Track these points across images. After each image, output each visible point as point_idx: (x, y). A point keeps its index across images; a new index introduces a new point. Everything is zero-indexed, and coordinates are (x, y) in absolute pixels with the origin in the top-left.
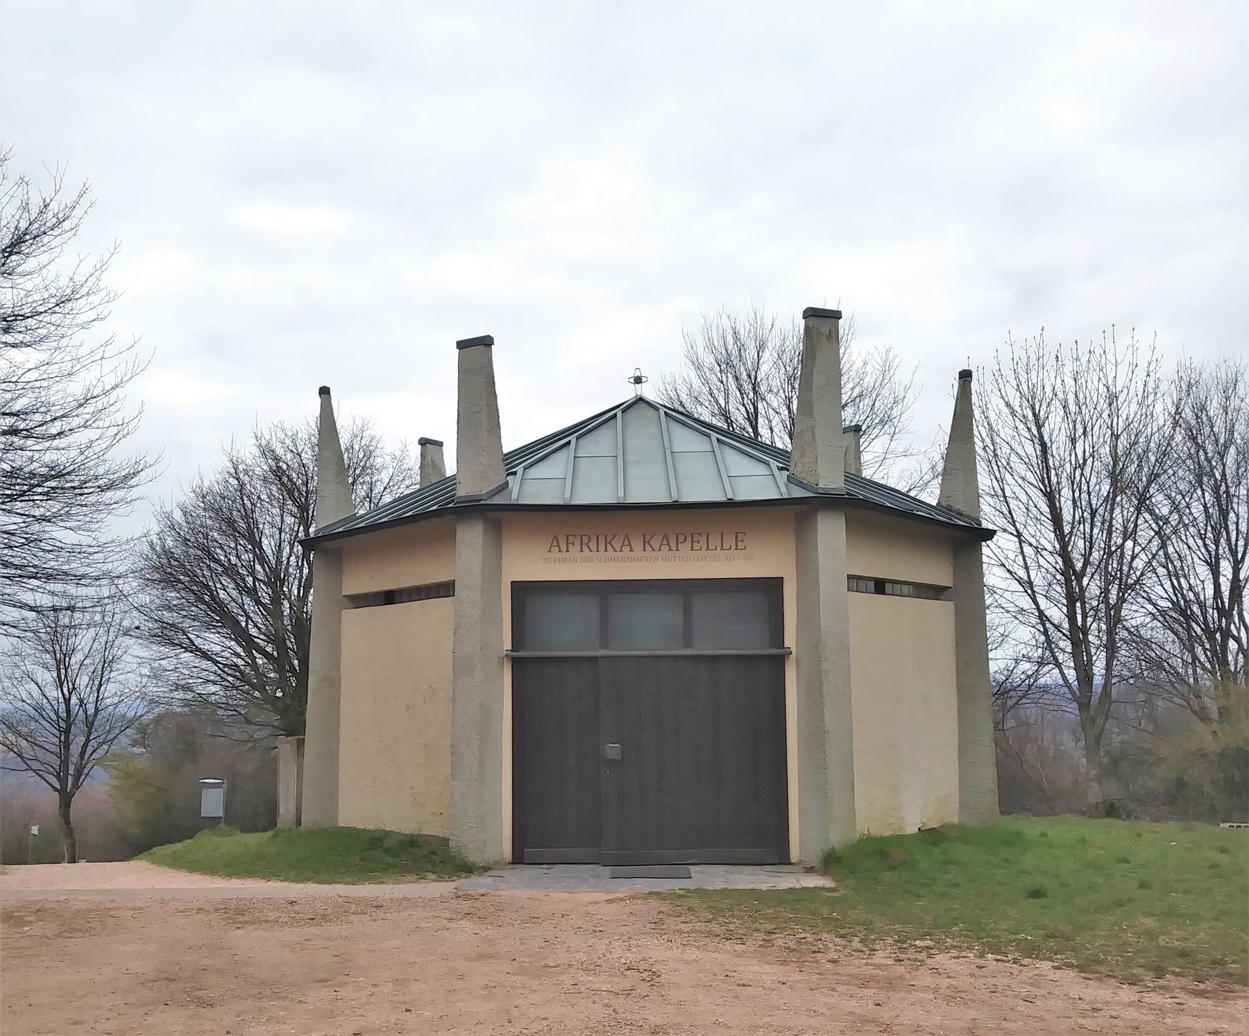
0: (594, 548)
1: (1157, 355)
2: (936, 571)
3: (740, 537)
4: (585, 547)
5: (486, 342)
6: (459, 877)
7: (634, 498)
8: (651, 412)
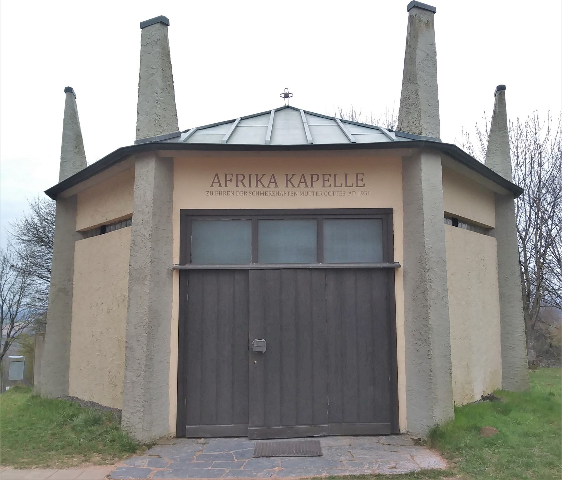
0: (247, 184)
2: (484, 215)
3: (360, 177)
4: (240, 183)
5: (163, 22)
6: (120, 458)
7: (279, 141)
8: (296, 113)
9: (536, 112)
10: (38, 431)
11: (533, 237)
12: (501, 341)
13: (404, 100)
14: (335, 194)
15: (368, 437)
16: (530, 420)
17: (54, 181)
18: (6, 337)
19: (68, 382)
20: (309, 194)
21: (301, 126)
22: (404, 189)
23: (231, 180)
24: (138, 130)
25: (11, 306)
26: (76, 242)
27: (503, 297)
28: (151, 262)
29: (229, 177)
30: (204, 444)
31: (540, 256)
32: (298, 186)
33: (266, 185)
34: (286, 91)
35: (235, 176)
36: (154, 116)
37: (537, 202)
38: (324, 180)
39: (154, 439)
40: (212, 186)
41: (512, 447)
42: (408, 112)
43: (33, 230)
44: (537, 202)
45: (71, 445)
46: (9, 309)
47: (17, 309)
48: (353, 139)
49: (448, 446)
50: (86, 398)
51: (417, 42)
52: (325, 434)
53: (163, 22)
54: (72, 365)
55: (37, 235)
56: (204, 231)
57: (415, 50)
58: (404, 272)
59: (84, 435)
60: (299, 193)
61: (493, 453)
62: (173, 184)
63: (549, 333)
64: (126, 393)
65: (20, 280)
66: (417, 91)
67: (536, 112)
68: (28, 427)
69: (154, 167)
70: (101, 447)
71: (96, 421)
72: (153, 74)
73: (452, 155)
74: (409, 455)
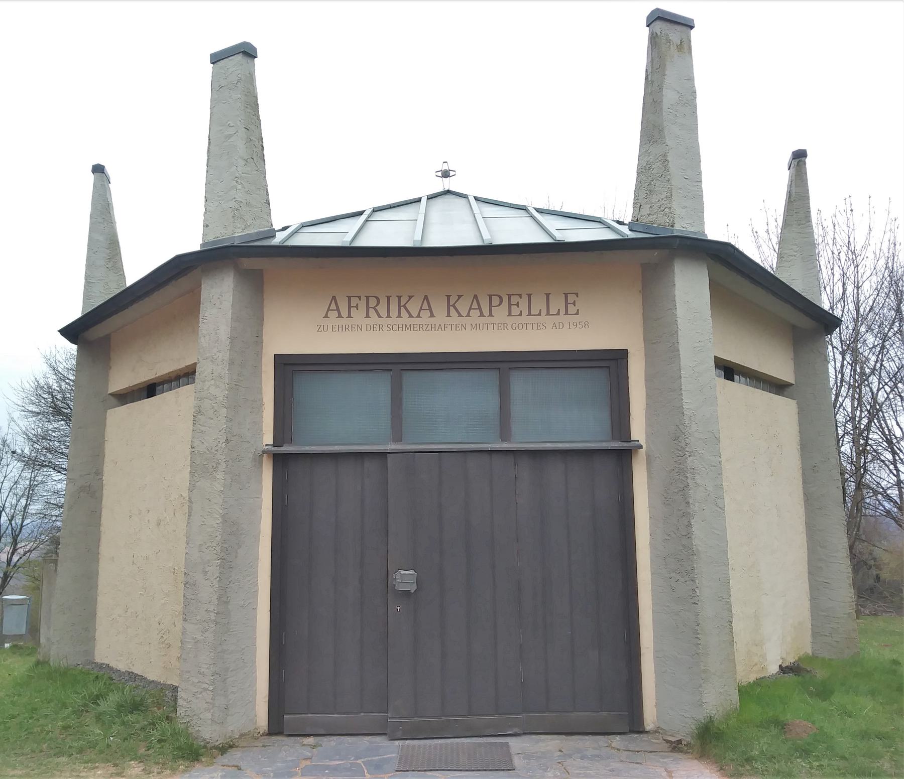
0: (384, 313)
1: (892, 216)
2: (776, 363)
3: (571, 298)
4: (372, 311)
5: (247, 52)
7: (435, 240)
8: (462, 201)
9: (848, 199)
10: (42, 721)
11: (848, 403)
12: (809, 573)
13: (643, 170)
14: (530, 327)
15: (591, 737)
16: (869, 710)
17: (74, 312)
18: (5, 565)
19: (94, 639)
20: (485, 327)
21: (471, 219)
22: (646, 319)
23: (357, 307)
24: (206, 226)
25: (13, 517)
26: (110, 412)
27: (811, 502)
28: (227, 441)
29: (354, 302)
30: (314, 747)
31: (859, 436)
32: (468, 315)
33: (415, 314)
34: (445, 167)
35: (364, 299)
36: (233, 204)
37: (851, 348)
38: (510, 305)
39: (230, 737)
40: (326, 316)
41: (843, 758)
42: (650, 191)
43: (46, 396)
44: (851, 348)
45: (94, 747)
46: (10, 521)
47: (23, 522)
48: (560, 236)
49: (730, 755)
50: (122, 667)
51: (664, 75)
52: (516, 730)
53: (247, 52)
54: (100, 613)
55: (54, 406)
56: (312, 390)
57: (661, 89)
58: (648, 457)
59: (115, 728)
60: (469, 327)
61: (811, 768)
62: (262, 320)
63: (875, 559)
64: (185, 660)
65: (27, 474)
66: (665, 155)
67: (848, 199)
68: (27, 715)
69: (232, 286)
70: (142, 751)
71: (136, 707)
72: (230, 136)
73: (724, 258)
74: (663, 769)
